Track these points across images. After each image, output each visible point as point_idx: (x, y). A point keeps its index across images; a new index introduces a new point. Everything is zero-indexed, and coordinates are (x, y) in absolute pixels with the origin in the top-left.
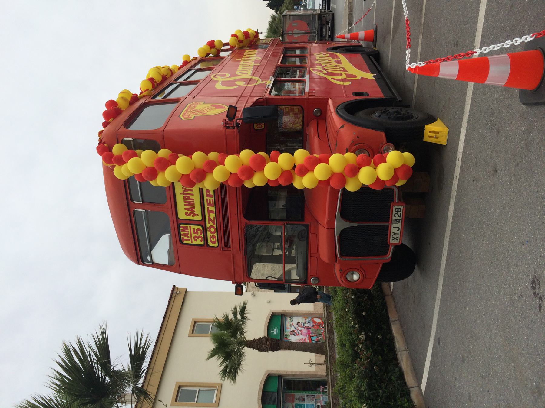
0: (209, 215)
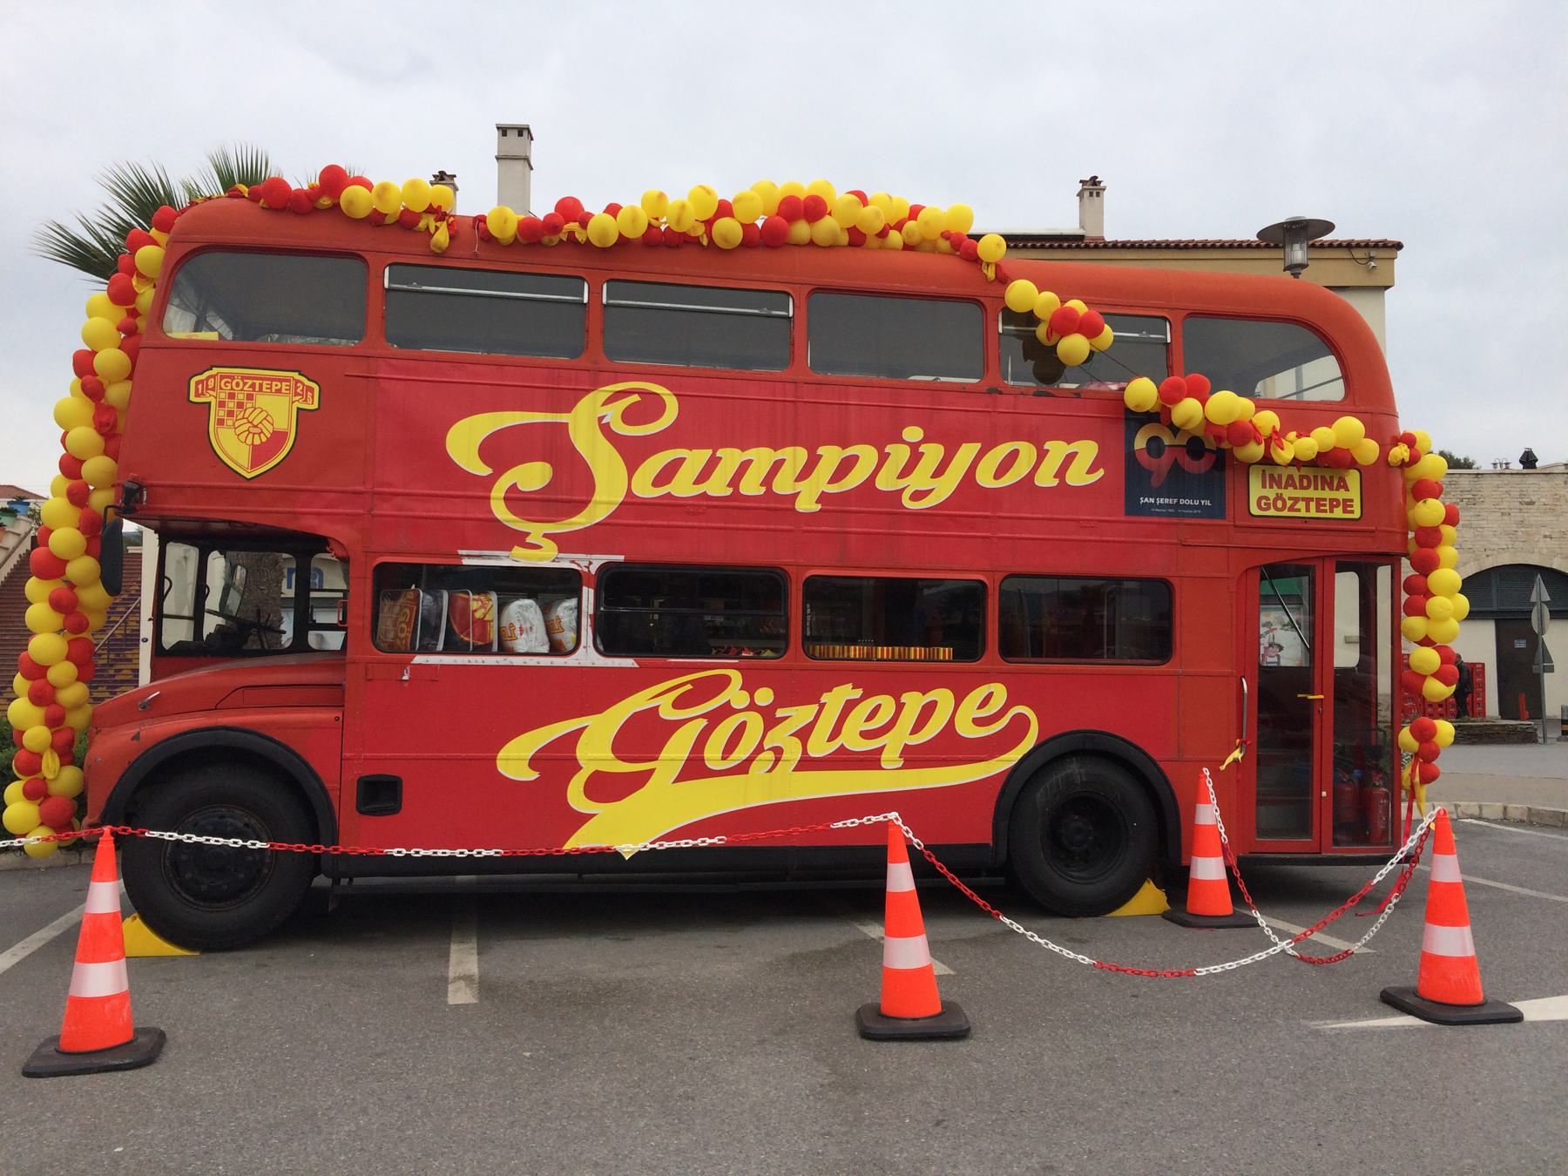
0: (1303, 499)
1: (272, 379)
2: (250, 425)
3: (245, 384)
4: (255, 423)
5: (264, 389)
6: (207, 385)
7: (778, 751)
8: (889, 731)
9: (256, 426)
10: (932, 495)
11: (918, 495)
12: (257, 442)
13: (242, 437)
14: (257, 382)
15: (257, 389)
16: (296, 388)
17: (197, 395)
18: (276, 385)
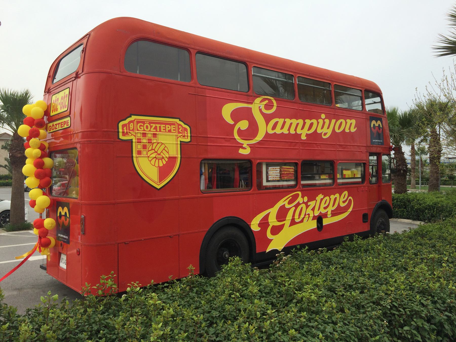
1: (166, 124)
2: (156, 154)
3: (151, 127)
4: (159, 152)
5: (162, 130)
6: (129, 128)
7: (309, 214)
8: (328, 207)
9: (159, 154)
10: (328, 134)
11: (325, 134)
12: (161, 165)
13: (153, 162)
14: (158, 125)
15: (158, 130)
16: (179, 129)
17: (124, 134)
18: (168, 127)
